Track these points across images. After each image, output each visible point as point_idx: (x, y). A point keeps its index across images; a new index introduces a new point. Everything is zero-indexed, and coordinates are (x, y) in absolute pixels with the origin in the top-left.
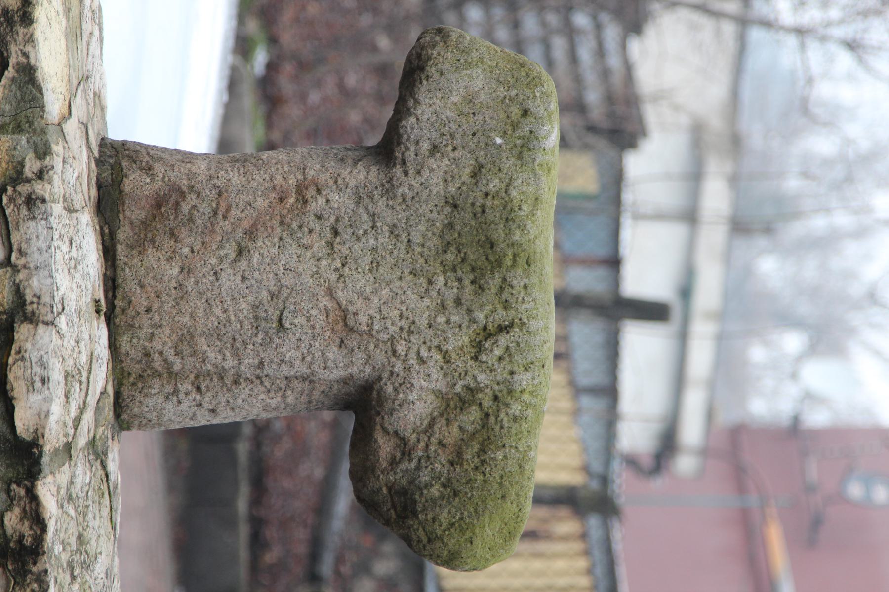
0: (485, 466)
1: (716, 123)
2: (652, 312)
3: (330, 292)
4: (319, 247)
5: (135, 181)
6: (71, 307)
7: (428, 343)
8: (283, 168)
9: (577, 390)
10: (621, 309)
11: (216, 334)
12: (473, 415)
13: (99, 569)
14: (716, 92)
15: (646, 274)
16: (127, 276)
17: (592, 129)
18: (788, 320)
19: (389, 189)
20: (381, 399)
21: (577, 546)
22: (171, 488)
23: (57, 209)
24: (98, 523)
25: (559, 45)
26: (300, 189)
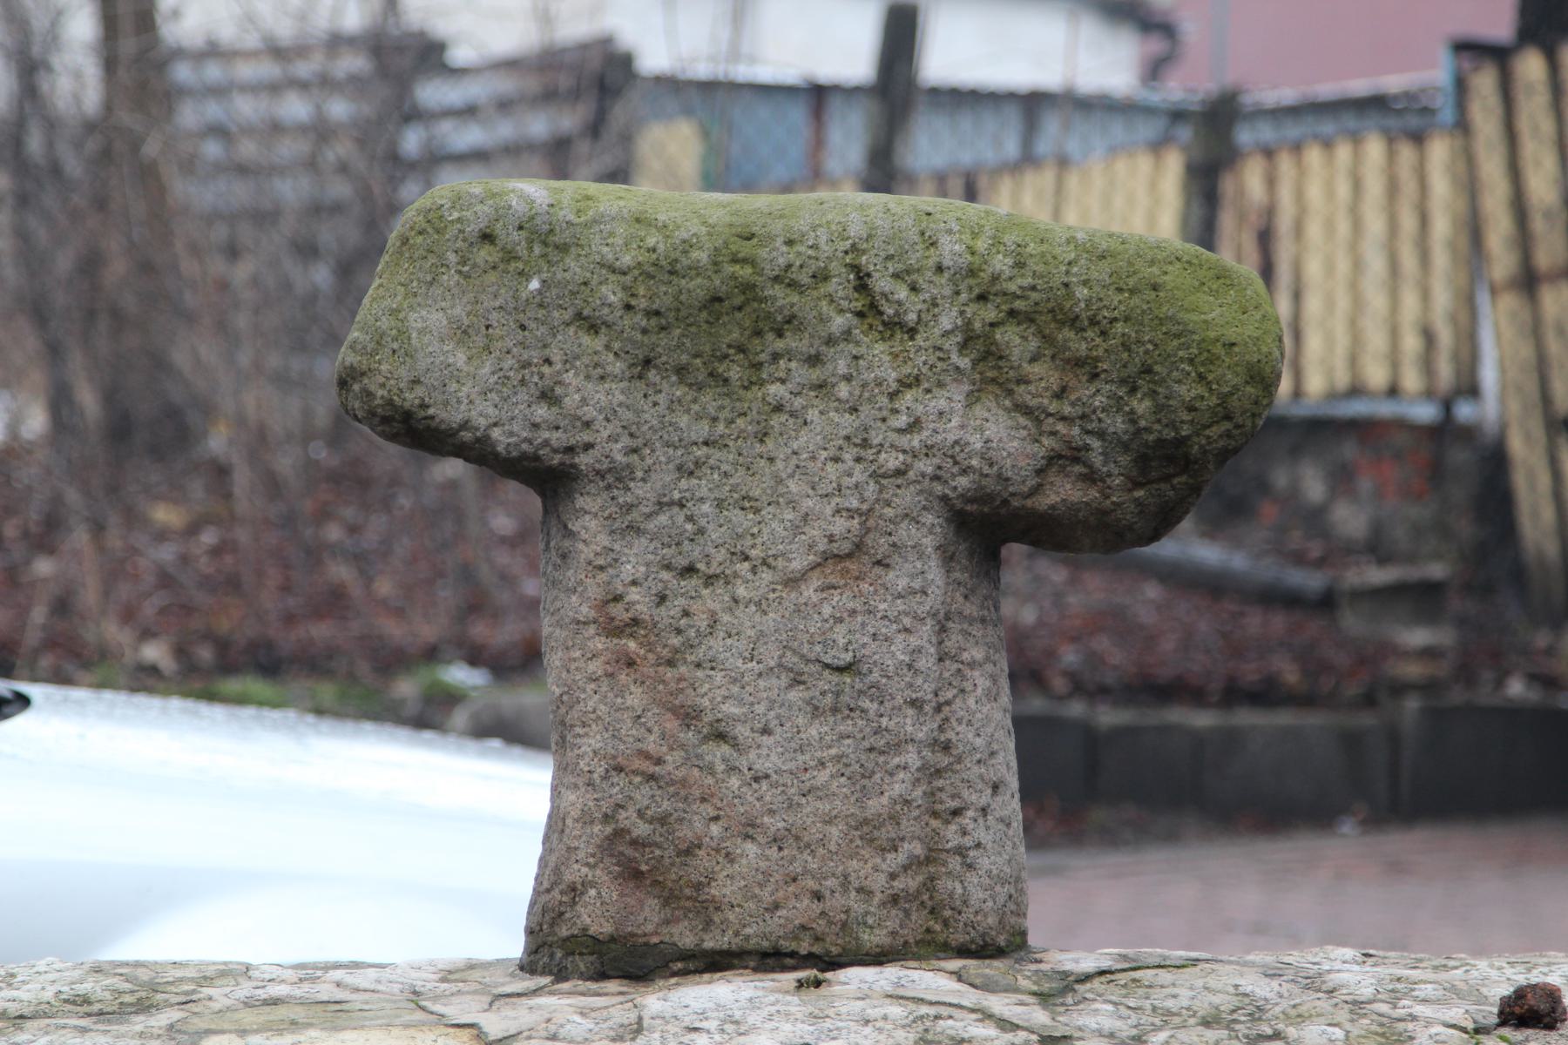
0: (1099, 317)
3: (793, 582)
4: (712, 600)
7: (885, 413)
12: (1012, 338)
13: (1263, 989)
16: (757, 932)
21: (1285, 164)
22: (1171, 837)
26: (614, 630)
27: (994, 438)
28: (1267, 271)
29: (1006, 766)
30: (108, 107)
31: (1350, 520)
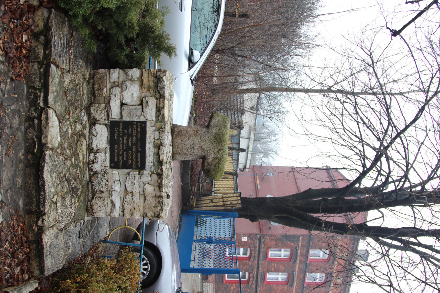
1: (252, 127)
2: (243, 150)
3: (200, 144)
4: (199, 138)
5: (176, 129)
6: (167, 144)
11: (185, 149)
12: (217, 160)
13: (170, 178)
14: (253, 122)
15: (243, 145)
16: (175, 141)
17: (236, 127)
18: (261, 152)
19: (208, 131)
20: (206, 158)
22: (181, 170)
23: (166, 132)
24: (170, 172)
25: (233, 116)
26: (197, 131)
27: (210, 159)
28: (224, 178)
29: (186, 159)
30: (239, 89)
31: (205, 184)
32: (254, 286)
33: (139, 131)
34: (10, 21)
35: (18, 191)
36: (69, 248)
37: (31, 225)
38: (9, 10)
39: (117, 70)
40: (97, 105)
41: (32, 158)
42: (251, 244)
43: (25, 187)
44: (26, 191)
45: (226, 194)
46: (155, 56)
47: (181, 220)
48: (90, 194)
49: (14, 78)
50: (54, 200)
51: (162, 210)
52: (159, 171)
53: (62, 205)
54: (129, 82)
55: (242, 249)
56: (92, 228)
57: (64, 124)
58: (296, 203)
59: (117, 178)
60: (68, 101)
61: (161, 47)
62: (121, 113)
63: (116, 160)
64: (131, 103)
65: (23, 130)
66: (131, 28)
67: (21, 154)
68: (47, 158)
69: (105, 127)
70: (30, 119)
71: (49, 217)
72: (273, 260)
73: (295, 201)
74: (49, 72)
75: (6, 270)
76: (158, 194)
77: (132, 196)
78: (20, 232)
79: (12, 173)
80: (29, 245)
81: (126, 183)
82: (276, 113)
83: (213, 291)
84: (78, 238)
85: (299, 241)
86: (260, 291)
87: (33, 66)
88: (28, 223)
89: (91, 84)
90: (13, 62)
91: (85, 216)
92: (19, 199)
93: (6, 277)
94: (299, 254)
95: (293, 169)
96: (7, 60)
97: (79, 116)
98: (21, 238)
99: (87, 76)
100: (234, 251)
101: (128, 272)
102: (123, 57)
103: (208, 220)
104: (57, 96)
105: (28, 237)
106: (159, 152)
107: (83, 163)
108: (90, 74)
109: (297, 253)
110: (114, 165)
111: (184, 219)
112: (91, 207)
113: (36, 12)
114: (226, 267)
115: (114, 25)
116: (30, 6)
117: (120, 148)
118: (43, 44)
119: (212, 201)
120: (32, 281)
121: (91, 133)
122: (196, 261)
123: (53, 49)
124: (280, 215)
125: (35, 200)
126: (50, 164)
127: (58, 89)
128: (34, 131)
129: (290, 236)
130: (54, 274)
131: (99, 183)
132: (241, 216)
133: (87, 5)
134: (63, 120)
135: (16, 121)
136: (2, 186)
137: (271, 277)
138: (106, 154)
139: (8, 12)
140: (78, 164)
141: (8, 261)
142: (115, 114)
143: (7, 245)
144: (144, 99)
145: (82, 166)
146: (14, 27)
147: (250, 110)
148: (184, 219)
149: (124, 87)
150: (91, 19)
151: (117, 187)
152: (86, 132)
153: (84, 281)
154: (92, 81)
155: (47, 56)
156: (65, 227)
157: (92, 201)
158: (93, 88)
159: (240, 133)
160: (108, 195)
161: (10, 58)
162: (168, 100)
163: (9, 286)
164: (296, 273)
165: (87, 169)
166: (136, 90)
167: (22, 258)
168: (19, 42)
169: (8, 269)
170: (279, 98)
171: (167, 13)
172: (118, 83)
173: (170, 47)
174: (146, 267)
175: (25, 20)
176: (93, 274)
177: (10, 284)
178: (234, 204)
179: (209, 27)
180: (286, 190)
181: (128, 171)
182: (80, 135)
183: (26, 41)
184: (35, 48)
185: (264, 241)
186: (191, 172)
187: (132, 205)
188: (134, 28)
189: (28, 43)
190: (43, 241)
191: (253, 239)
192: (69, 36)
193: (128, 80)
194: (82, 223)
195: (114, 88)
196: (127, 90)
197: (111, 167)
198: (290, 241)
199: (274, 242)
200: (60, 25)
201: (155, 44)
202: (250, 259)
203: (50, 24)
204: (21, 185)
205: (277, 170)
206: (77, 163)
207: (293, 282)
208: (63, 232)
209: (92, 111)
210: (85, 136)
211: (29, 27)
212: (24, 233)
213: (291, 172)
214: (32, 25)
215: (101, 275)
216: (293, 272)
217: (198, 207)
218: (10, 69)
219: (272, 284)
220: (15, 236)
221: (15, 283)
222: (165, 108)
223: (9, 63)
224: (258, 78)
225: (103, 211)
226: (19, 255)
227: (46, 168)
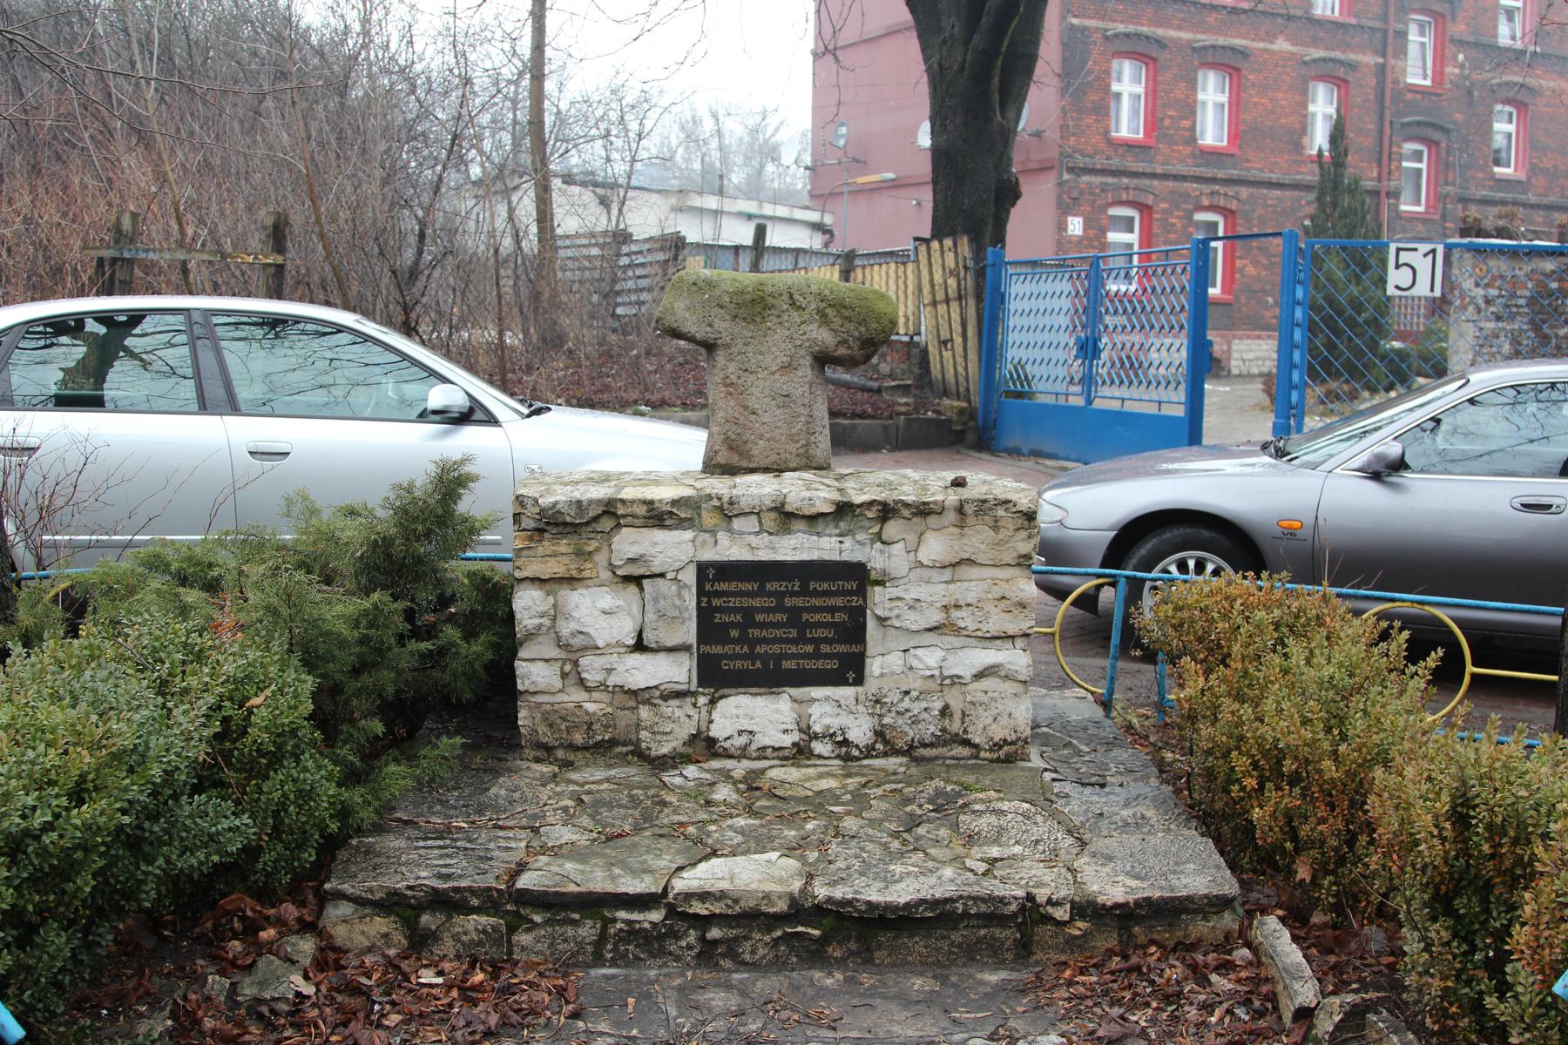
1: (673, 201)
2: (760, 232)
3: (773, 373)
4: (753, 378)
5: (722, 458)
8: (715, 393)
9: (795, 268)
10: (759, 245)
11: (790, 424)
12: (829, 311)
13: (892, 478)
15: (743, 234)
16: (763, 463)
17: (675, 258)
18: (760, 171)
19: (727, 346)
21: (868, 270)
23: (734, 492)
32: (1244, 192)
33: (733, 586)
34: (379, 1026)
35: (954, 985)
36: (1143, 817)
37: (1067, 942)
38: (341, 1029)
39: (521, 667)
40: (644, 734)
41: (840, 943)
42: (1094, 202)
43: (938, 963)
44: (953, 963)
45: (920, 289)
46: (470, 531)
47: (1015, 453)
48: (953, 753)
49: (571, 1007)
50: (981, 867)
51: (1008, 502)
52: (870, 514)
53: (996, 841)
54: (560, 623)
55: (1114, 237)
56: (1068, 745)
57: (717, 841)
58: (952, 36)
59: (895, 660)
60: (637, 829)
61: (440, 511)
62: (671, 650)
63: (833, 665)
64: (633, 618)
65: (745, 975)
66: (376, 617)
67: (829, 981)
68: (839, 893)
69: (722, 704)
70: (708, 954)
71: (1040, 885)
72: (1153, 123)
73: (944, 42)
74: (545, 893)
75: (1221, 1019)
76: (951, 516)
77: (958, 607)
78: (1094, 979)
79: (893, 1006)
80: (1137, 947)
81: (914, 628)
82: (620, 118)
83: (1259, 337)
84: (1107, 790)
85: (1085, 28)
86: (1261, 170)
87: (523, 949)
88: (1063, 951)
89: (571, 757)
90: (517, 1011)
91: (1030, 769)
92: (982, 983)
93: (1247, 1018)
94: (1131, 28)
95: (827, 51)
96: (512, 1031)
97: (686, 795)
98: (1112, 973)
99: (545, 769)
100: (1120, 262)
101: (1225, 616)
102: (474, 648)
103: (1012, 354)
104: (624, 865)
105: (1108, 950)
106: (804, 517)
107: (849, 775)
108: (538, 760)
109: (1127, 35)
110: (850, 670)
111: (1011, 441)
112: (998, 746)
113: (339, 942)
114: (1183, 288)
115: (366, 679)
116: (318, 964)
117: (794, 650)
118: (450, 917)
119: (945, 343)
120: (1257, 935)
121: (743, 753)
122: (1161, 394)
123: (464, 883)
124: (997, 95)
125: (983, 932)
126: (860, 882)
127: (601, 861)
128: (746, 938)
129: (1065, 61)
130: (1233, 866)
131: (915, 721)
132: (999, 238)
133: (306, 770)
134: (706, 845)
135: (718, 999)
136: (942, 1038)
137: (1212, 131)
138: (814, 700)
139: (347, 1032)
140: (850, 792)
141: (1192, 1013)
142: (677, 671)
143: (1140, 1018)
144: (619, 572)
145: (857, 779)
146: (398, 1013)
147: (615, 211)
148: (1011, 441)
149: (577, 642)
150: (351, 758)
151: (930, 658)
152: (739, 768)
153: (1255, 765)
154: (560, 754)
155: (490, 901)
156: (1069, 832)
157: (976, 746)
158: (586, 748)
159: (698, 245)
160: (956, 690)
161: (505, 1023)
162: (620, 488)
163: (1276, 1008)
164: (1199, 37)
165: (865, 762)
166: (588, 601)
167: (1179, 970)
168: (446, 994)
169: (1217, 1013)
170: (564, 106)
171: (305, 498)
172: (564, 661)
173: (441, 480)
174: (1191, 564)
175: (370, 978)
176: (1230, 736)
177: (1269, 1006)
178: (957, 263)
179: (330, 355)
180: (904, 75)
181: (871, 624)
182: (751, 789)
183: (440, 973)
184: (463, 944)
185: (1083, 155)
186: (844, 416)
187: (989, 607)
188: (375, 607)
189: (447, 966)
190: (1121, 900)
191: (1075, 194)
192: (413, 833)
193: (554, 627)
194: (1054, 775)
195: (584, 675)
196: (591, 631)
197: (859, 681)
198: (1084, 62)
199: (1089, 120)
200: (377, 860)
201: (428, 534)
202: (1149, 208)
203: (378, 896)
204: (934, 977)
205: (828, 110)
206: (849, 797)
207: (1233, 49)
208: (1087, 837)
209: (665, 750)
210: (754, 772)
211: (391, 964)
212: (1094, 966)
213: (836, 58)
214: (385, 956)
215: (1236, 706)
216: (1194, 49)
217: (968, 389)
218: (542, 1020)
219: (1237, 126)
220: (1105, 993)
221: (1265, 989)
222: (649, 497)
223: (523, 1027)
224: (498, 183)
225: (1010, 705)
226: (1169, 979)
227: (875, 897)
